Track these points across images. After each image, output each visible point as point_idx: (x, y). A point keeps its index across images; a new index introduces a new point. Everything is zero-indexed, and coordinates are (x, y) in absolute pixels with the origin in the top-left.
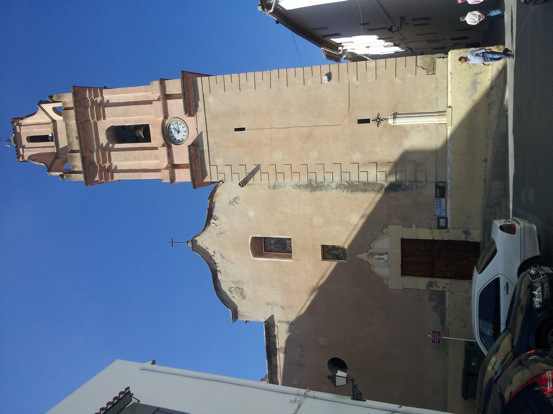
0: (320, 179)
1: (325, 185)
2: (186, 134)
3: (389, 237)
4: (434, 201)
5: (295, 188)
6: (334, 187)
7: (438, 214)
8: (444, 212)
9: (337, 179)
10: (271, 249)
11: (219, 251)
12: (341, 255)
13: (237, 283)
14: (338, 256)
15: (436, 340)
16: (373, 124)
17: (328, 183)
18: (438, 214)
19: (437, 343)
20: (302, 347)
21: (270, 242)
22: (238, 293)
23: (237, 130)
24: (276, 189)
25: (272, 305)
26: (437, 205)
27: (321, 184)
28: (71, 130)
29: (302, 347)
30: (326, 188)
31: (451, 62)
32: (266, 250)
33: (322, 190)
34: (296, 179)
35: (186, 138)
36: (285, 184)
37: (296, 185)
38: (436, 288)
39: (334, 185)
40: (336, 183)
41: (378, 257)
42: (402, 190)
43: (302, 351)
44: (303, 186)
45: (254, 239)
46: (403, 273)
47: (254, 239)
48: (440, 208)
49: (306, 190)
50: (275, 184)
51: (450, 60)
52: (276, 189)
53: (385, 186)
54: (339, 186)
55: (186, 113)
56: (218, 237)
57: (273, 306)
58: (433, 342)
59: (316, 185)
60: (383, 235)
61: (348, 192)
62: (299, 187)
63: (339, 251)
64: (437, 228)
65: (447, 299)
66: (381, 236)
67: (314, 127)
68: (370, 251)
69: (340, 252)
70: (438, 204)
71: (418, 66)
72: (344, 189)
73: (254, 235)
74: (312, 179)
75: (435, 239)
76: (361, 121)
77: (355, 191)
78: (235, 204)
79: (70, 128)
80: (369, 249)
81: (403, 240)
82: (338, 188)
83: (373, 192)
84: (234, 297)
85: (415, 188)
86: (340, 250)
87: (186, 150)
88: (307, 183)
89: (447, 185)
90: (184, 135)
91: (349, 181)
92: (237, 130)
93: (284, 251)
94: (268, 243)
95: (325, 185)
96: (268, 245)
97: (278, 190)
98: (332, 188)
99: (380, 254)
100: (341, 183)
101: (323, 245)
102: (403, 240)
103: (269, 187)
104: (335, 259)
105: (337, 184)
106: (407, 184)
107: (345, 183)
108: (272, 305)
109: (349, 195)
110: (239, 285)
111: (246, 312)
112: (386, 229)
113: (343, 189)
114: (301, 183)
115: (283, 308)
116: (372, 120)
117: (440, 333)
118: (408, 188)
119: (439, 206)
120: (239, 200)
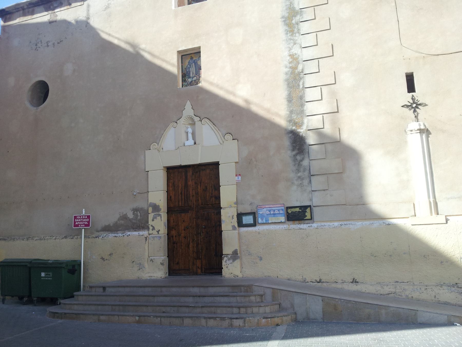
4: (280, 206)
6: (292, 51)
8: (265, 222)
12: (190, 80)
15: (78, 221)
16: (407, 97)
19: (75, 222)
20: (58, 43)
27: (296, 30)
29: (58, 43)
30: (290, 39)
33: (287, 34)
38: (151, 216)
39: (296, 50)
41: (189, 132)
42: (295, 156)
43: (54, 44)
44: (291, 3)
46: (170, 170)
48: (270, 214)
49: (284, 9)
58: (75, 217)
61: (286, 74)
63: (194, 77)
64: (239, 212)
65: (138, 232)
67: (394, 4)
68: (196, 119)
69: (192, 78)
75: (222, 210)
76: (410, 79)
77: (288, 84)
80: (200, 118)
81: (216, 165)
83: (288, 113)
86: (197, 77)
89: (307, 224)
91: (304, 73)
95: (295, 38)
98: (290, 49)
99: (193, 134)
100: (300, 62)
102: (216, 165)
104: (183, 72)
106: (305, 163)
107: (300, 67)
113: (291, 65)
117: (88, 225)
118: (298, 164)
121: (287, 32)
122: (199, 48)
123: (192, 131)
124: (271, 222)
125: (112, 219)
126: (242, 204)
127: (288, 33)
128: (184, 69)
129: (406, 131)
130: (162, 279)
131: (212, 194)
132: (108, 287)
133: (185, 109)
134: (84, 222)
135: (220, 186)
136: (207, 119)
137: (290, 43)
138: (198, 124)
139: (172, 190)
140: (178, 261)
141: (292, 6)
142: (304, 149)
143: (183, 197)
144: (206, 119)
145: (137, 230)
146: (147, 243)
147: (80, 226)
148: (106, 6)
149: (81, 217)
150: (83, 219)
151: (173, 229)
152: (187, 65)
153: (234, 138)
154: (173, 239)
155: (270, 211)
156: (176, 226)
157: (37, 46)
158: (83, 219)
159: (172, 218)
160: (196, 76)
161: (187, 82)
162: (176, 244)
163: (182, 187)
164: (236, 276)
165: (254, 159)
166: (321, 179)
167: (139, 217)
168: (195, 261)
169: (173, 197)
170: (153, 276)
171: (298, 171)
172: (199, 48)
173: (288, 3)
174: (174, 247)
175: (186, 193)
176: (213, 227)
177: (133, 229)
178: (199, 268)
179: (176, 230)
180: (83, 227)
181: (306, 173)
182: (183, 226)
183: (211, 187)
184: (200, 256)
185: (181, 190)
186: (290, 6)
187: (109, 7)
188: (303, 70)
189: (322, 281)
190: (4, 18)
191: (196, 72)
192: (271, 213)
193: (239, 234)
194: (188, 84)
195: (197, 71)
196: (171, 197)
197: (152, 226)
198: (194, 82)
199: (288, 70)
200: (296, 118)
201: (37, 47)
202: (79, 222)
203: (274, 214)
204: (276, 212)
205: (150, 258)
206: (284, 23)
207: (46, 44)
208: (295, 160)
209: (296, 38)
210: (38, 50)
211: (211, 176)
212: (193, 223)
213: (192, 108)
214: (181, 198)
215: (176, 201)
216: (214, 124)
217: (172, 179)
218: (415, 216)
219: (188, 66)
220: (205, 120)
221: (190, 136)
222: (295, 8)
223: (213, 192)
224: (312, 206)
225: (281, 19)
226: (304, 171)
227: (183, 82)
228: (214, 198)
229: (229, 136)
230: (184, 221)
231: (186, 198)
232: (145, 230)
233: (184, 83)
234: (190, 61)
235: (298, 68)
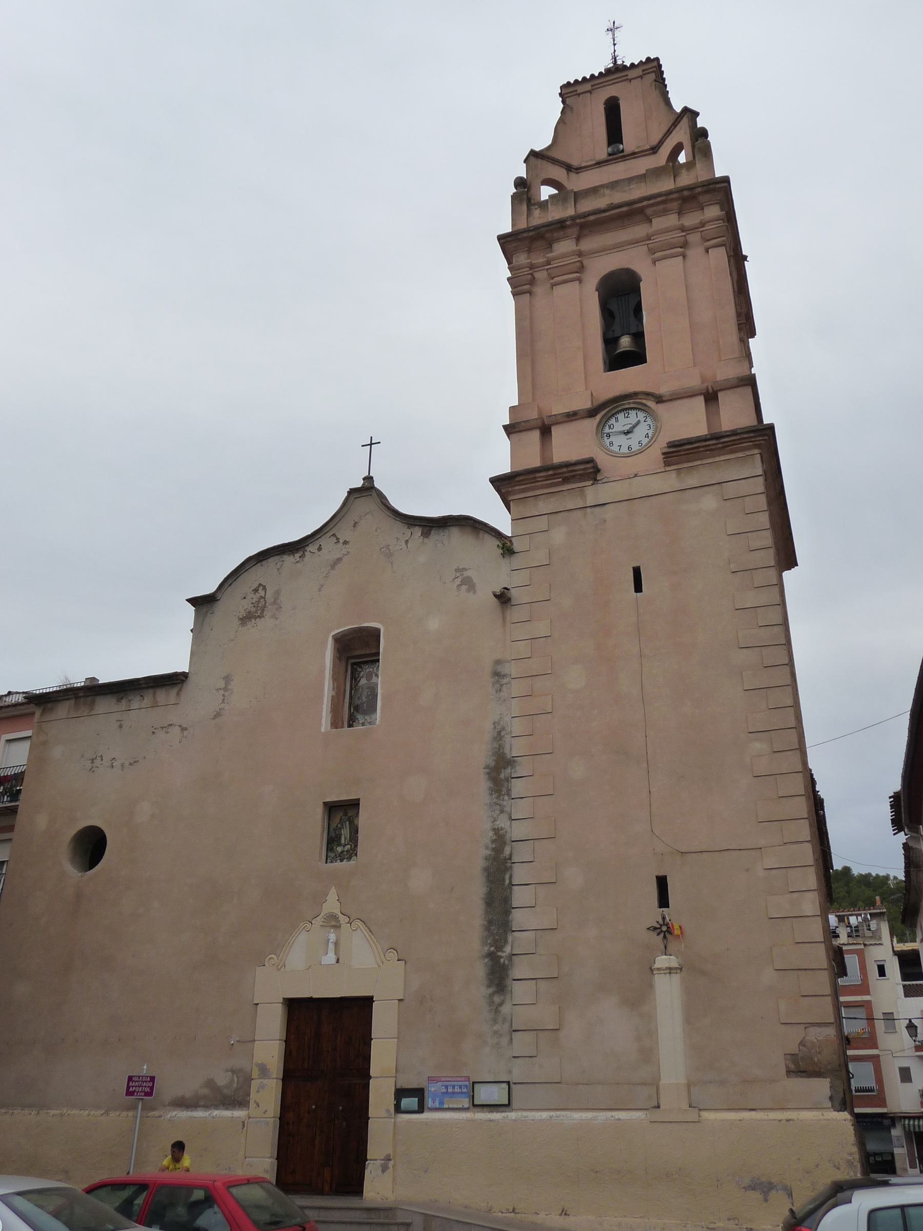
0: (518, 787)
1: (503, 800)
2: (624, 450)
3: (377, 966)
4: (463, 1079)
5: (495, 727)
7: (433, 1089)
8: (438, 1106)
9: (517, 831)
10: (358, 680)
11: (348, 553)
12: (339, 849)
13: (275, 602)
14: (335, 844)
15: (134, 1084)
16: (654, 914)
17: (507, 809)
18: (433, 1089)
19: (128, 1087)
20: (131, 764)
21: (374, 675)
22: (254, 606)
23: (637, 572)
24: (493, 680)
25: (225, 689)
26: (454, 1087)
27: (504, 791)
28: (627, 189)
29: (131, 764)
30: (496, 804)
31: (819, 1120)
32: (355, 666)
33: (491, 794)
34: (517, 727)
35: (613, 452)
36: (505, 700)
37: (503, 729)
38: (255, 1085)
39: (503, 822)
40: (509, 830)
41: (331, 941)
42: (491, 995)
43: (123, 765)
44: (500, 745)
45: (375, 635)
46: (294, 1006)
47: (375, 635)
48: (447, 1093)
49: (490, 753)
50: (504, 676)
51: (824, 1118)
52: (493, 680)
53: (500, 954)
54: (500, 839)
55: (671, 445)
56: (380, 549)
57: (222, 692)
58: (130, 1079)
59: (503, 778)
60: (380, 951)
61: (486, 859)
62: (499, 736)
63: (348, 844)
64: (398, 1087)
65: (231, 1112)
66: (378, 945)
67: (645, 765)
68: (343, 919)
69: (344, 846)
70: (457, 1090)
71: (805, 1028)
72: (493, 849)
73: (384, 633)
74: (518, 768)
75: (371, 1081)
76: (662, 883)
77: (488, 876)
78: (458, 581)
79: (631, 187)
80: (349, 917)
82: (495, 834)
84: (245, 598)
85: (496, 1028)
86: (351, 845)
87: (584, 455)
88: (509, 756)
89: (502, 1112)
90: (621, 446)
92: (637, 572)
93: (352, 711)
94: (371, 670)
96: (367, 670)
97: (491, 685)
99: (336, 944)
100: (508, 841)
101: (359, 804)
103: (498, 662)
104: (330, 835)
105: (506, 832)
106: (506, 1009)
108: (225, 689)
109: (478, 864)
110: (270, 607)
111: (212, 630)
112: (397, 959)
114: (508, 739)
115: (218, 715)
116: (663, 911)
117: (150, 1094)
119: (450, 1090)
120: (468, 591)
121: (492, 791)
122: (359, 800)
123: (336, 940)
124: (447, 1107)
125: (191, 1085)
127: (493, 793)
128: (331, 829)
129: (652, 968)
132: (711, 248)
133: (327, 900)
134: (144, 1088)
135: (372, 1039)
136: (360, 922)
137: (495, 811)
138: (345, 927)
141: (501, 750)
142: (506, 986)
144: (359, 920)
145: (229, 1106)
147: (137, 1094)
148: (217, 711)
149: (139, 1078)
150: (144, 1082)
152: (338, 824)
153: (399, 958)
155: (447, 1087)
157: (94, 765)
158: (142, 1081)
160: (350, 843)
161: (335, 852)
166: (528, 1037)
167: (236, 1084)
171: (495, 1021)
172: (359, 800)
173: (496, 745)
177: (224, 1104)
180: (142, 1096)
181: (507, 1026)
186: (497, 750)
187: (220, 715)
188: (511, 855)
189: (517, 1211)
190: (42, 708)
191: (350, 837)
192: (449, 1091)
194: (336, 855)
195: (353, 835)
196: (291, 1052)
198: (345, 853)
199: (490, 853)
200: (497, 933)
201: (93, 766)
202: (136, 1087)
203: (453, 1093)
204: (456, 1090)
205: (246, 1159)
206: (487, 776)
207: (110, 763)
208: (491, 1003)
209: (505, 803)
210: (94, 771)
213: (338, 900)
216: (370, 932)
218: (659, 1107)
219: (339, 825)
220: (358, 923)
221: (331, 946)
222: (505, 754)
224: (511, 1083)
225: (484, 770)
226: (504, 1020)
227: (329, 851)
229: (391, 954)
233: (330, 854)
234: (343, 817)
235: (505, 851)
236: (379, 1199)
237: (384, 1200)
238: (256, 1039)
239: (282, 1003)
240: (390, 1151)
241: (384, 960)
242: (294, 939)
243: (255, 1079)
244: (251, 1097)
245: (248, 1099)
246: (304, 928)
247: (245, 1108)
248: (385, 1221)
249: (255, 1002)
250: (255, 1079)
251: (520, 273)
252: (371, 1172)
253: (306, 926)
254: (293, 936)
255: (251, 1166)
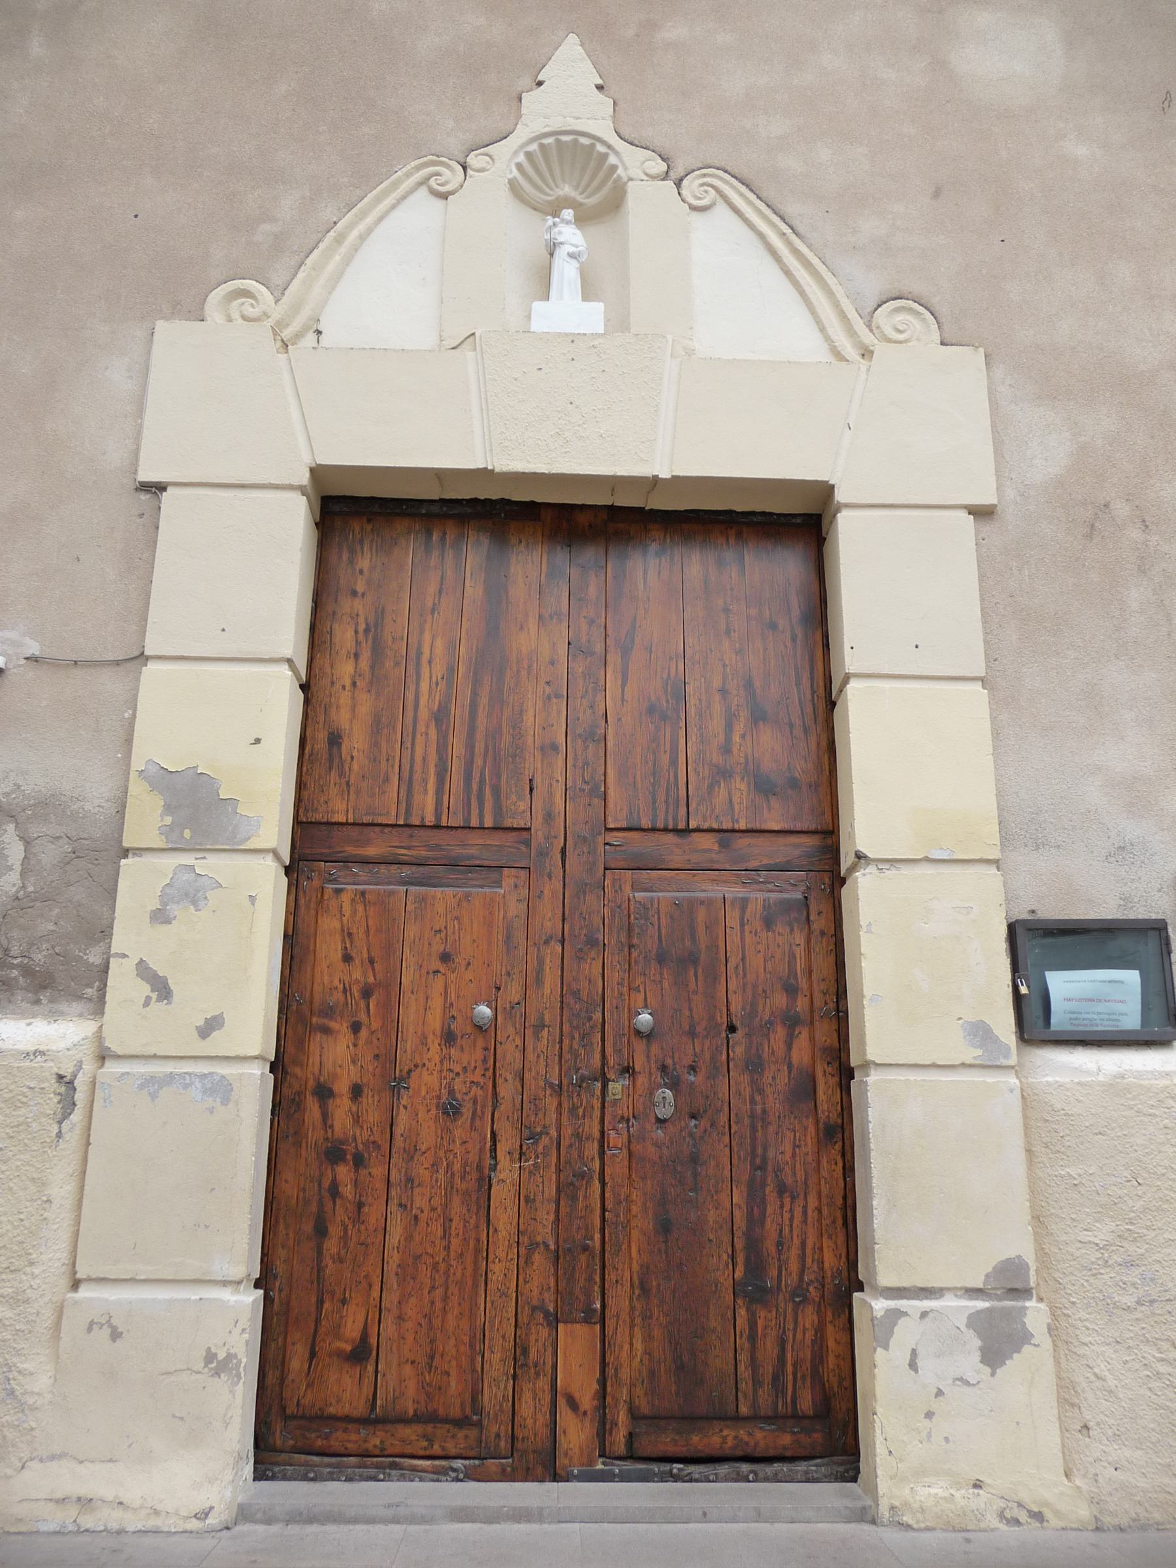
126: (1037, 848)
130: (211, 1531)
131: (727, 750)
133: (540, 84)
139: (354, 684)
140: (365, 1335)
143: (457, 749)
146: (72, 1137)
151: (333, 1025)
154: (325, 1116)
156: (367, 993)
159: (329, 924)
162: (359, 1161)
163: (451, 670)
164: (1023, 1516)
165: (1121, 510)
168: (544, 1332)
169: (356, 742)
170: (110, 1496)
174: (334, 1191)
175: (481, 715)
176: (732, 1029)
178: (573, 1404)
179: (364, 1033)
182: (437, 1003)
183: (723, 691)
184: (588, 1294)
185: (442, 686)
193: (1028, 1100)
196: (335, 740)
197: (144, 970)
211: (726, 610)
212: (539, 981)
214: (433, 758)
215: (387, 780)
217: (360, 588)
223: (736, 738)
228: (743, 786)
230: (445, 957)
231: (479, 761)
232: (63, 1006)
236: (993, 1521)
237: (1017, 1522)
238: (147, 653)
239: (302, 490)
240: (1022, 1247)
241: (868, 338)
242: (369, 220)
243: (139, 851)
244: (118, 943)
245: (94, 957)
246: (428, 179)
247: (77, 1007)
248: (919, 687)
249: (145, 476)
250: (139, 851)
251: (837, 305)
252: (913, 1365)
253: (438, 174)
254: (363, 214)
255: (115, 1335)
